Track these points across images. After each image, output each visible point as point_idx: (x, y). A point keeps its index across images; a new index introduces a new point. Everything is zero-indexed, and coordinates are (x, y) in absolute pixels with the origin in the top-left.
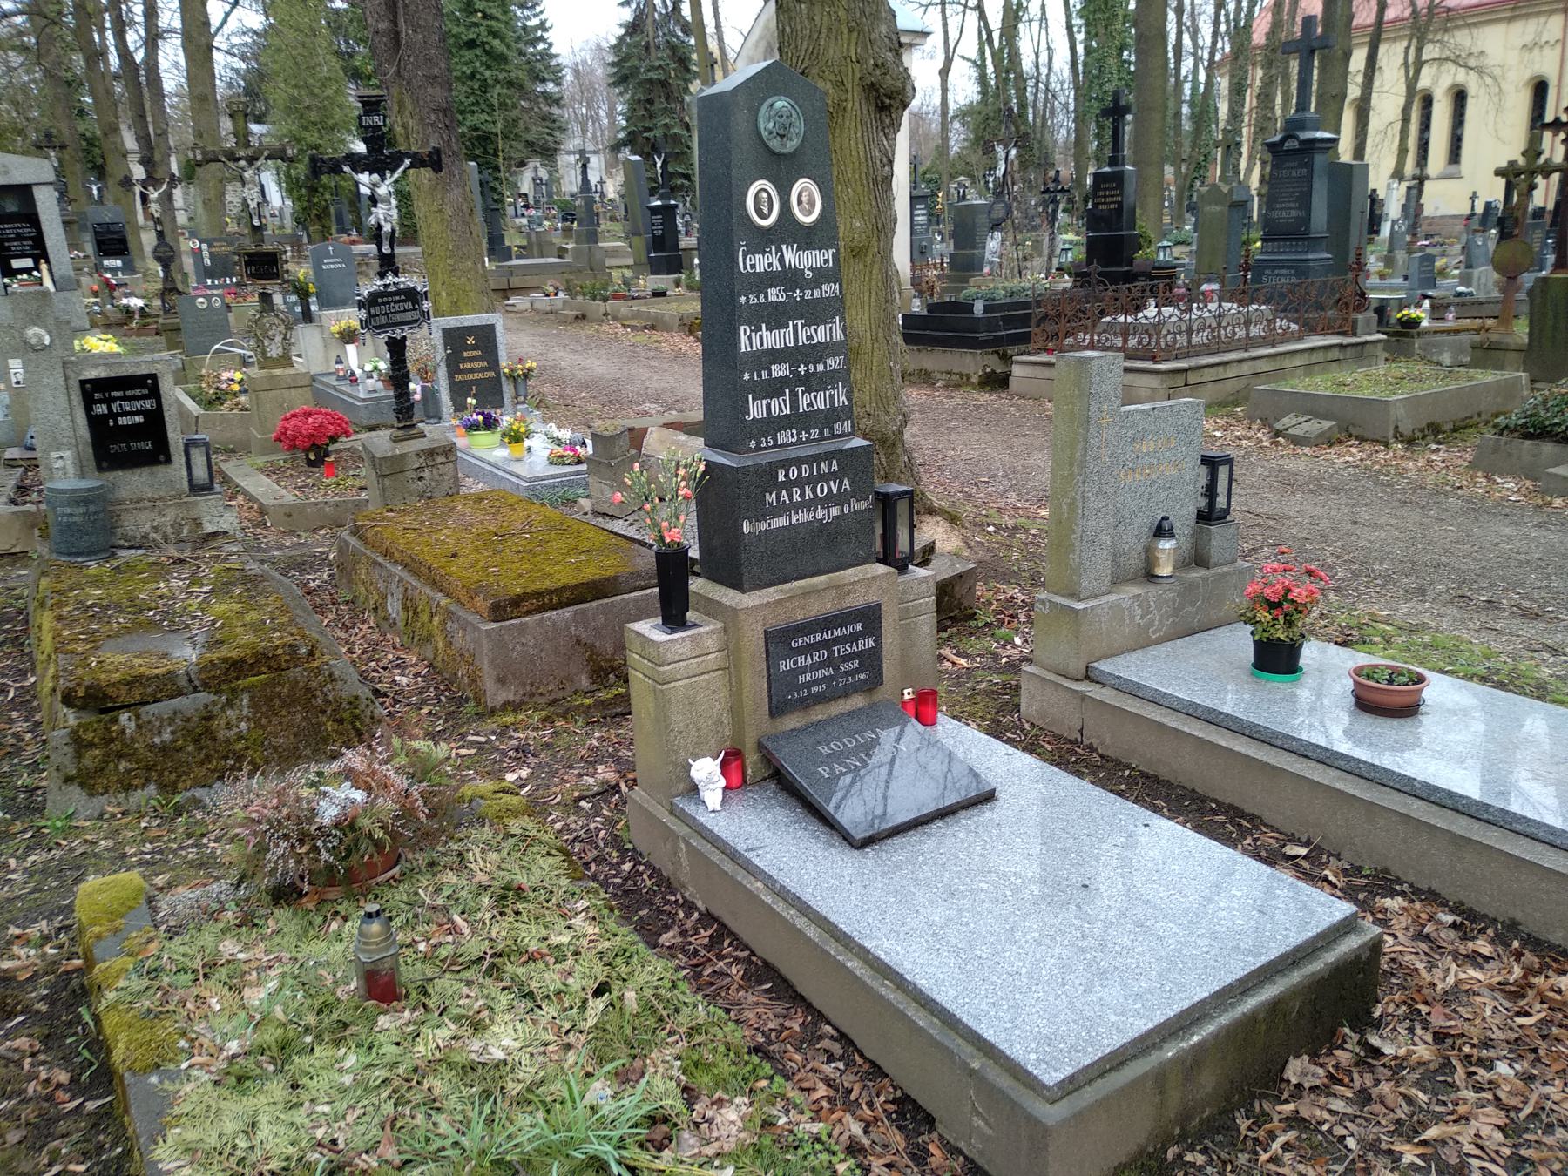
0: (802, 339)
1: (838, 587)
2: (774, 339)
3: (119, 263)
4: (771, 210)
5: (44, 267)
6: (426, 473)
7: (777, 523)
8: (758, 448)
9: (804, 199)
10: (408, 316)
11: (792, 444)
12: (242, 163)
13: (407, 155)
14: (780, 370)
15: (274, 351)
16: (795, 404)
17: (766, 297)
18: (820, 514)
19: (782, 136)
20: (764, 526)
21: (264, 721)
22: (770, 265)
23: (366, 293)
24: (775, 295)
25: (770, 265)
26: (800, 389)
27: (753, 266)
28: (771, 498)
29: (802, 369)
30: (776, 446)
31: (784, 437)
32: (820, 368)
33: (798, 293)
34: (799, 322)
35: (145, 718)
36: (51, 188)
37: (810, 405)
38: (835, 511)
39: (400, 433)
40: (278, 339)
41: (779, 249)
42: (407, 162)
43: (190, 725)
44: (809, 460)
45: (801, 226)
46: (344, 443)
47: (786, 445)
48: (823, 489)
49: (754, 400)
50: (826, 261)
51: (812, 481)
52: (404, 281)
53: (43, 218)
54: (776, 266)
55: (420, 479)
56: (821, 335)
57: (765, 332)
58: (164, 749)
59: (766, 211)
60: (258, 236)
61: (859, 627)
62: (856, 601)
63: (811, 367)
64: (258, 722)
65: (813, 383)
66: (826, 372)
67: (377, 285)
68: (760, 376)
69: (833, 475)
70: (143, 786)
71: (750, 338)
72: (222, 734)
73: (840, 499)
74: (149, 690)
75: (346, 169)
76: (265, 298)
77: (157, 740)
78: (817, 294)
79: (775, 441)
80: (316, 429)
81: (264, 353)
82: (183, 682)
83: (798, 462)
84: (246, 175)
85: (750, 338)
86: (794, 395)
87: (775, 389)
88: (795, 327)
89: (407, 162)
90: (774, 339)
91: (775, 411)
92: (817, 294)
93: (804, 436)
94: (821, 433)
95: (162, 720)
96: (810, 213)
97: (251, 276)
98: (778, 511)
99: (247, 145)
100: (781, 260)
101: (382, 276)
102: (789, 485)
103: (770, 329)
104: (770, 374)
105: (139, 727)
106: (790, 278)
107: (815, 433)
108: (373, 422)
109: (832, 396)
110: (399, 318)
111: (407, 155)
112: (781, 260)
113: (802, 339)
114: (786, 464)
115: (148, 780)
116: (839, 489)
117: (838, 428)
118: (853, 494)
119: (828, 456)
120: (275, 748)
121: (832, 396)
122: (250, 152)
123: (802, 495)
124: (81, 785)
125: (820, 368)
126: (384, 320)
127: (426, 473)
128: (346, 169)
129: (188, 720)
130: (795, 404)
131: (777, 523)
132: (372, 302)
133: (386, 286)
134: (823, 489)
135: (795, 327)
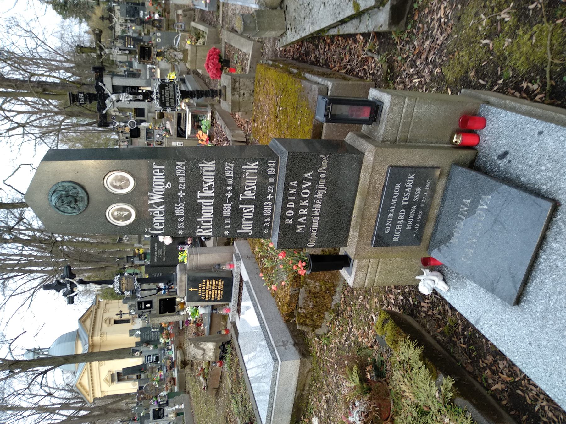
0: (210, 193)
1: (368, 195)
2: (207, 214)
3: (142, 12)
4: (126, 210)
5: (142, 88)
6: (242, 92)
7: (315, 226)
8: (269, 228)
9: (118, 184)
10: (171, 89)
11: (272, 206)
12: (102, 53)
13: (97, 83)
14: (227, 210)
15: (180, 56)
16: (249, 202)
17: (181, 217)
18: (320, 195)
19: (76, 201)
20: (315, 233)
21: (318, 278)
22: (161, 213)
23: (160, 108)
24: (180, 211)
25: (161, 213)
26: (241, 198)
27: (161, 224)
28: (300, 228)
29: (229, 195)
30: (271, 216)
31: (267, 210)
32: (231, 181)
33: (181, 194)
34: (199, 195)
35: (302, 306)
36: (113, 79)
37: (252, 190)
38: (322, 184)
39: (222, 97)
40: (176, 53)
41: (151, 206)
42: (100, 84)
43: (310, 297)
44: (285, 201)
45: (136, 186)
46: (223, 54)
47: (272, 210)
48: (306, 193)
49: (241, 229)
50: (161, 171)
51: (299, 199)
52: (155, 90)
53: (125, 84)
54: (162, 208)
55: (244, 94)
56: (209, 179)
57: (202, 219)
58: (314, 306)
59: (126, 213)
60: (133, 52)
61: (398, 186)
62: (380, 180)
63: (229, 188)
64: (317, 280)
65: (238, 190)
66: (234, 178)
67: (156, 103)
68: (228, 224)
69: (299, 188)
70: (324, 315)
71: (204, 229)
72: (317, 290)
73: (315, 180)
74: (294, 301)
75: (104, 112)
76: (159, 54)
77: (311, 306)
78: (182, 180)
79: (268, 216)
80: (214, 67)
81: (181, 60)
82: (295, 292)
83: (285, 209)
84: (107, 53)
85: (204, 229)
86: (244, 202)
87: (237, 214)
88: (202, 198)
89: (100, 84)
90: (207, 214)
91: (251, 215)
92: (182, 180)
93: (270, 197)
94: (271, 184)
95: (305, 303)
96: (128, 180)
97: (149, 58)
98: (309, 223)
99: (94, 49)
100: (158, 204)
101: (152, 99)
102: (296, 216)
103: (201, 215)
104: (228, 217)
105: (304, 309)
106: (170, 198)
107: (270, 189)
108: (216, 6)
109: (251, 174)
110: (172, 93)
111: (97, 83)
112: (158, 204)
113: (210, 193)
114: (283, 217)
115: (323, 313)
116: (309, 180)
117: (271, 171)
118: (315, 170)
119: (287, 187)
120: (329, 279)
121: (251, 174)
122: (98, 49)
123: (304, 207)
124: (316, 328)
125: (231, 181)
126: (172, 100)
127: (242, 92)
128: (104, 112)
129: (308, 297)
130: (249, 202)
131: (315, 226)
132: (163, 104)
133: (157, 98)
134: (306, 193)
135: (202, 198)
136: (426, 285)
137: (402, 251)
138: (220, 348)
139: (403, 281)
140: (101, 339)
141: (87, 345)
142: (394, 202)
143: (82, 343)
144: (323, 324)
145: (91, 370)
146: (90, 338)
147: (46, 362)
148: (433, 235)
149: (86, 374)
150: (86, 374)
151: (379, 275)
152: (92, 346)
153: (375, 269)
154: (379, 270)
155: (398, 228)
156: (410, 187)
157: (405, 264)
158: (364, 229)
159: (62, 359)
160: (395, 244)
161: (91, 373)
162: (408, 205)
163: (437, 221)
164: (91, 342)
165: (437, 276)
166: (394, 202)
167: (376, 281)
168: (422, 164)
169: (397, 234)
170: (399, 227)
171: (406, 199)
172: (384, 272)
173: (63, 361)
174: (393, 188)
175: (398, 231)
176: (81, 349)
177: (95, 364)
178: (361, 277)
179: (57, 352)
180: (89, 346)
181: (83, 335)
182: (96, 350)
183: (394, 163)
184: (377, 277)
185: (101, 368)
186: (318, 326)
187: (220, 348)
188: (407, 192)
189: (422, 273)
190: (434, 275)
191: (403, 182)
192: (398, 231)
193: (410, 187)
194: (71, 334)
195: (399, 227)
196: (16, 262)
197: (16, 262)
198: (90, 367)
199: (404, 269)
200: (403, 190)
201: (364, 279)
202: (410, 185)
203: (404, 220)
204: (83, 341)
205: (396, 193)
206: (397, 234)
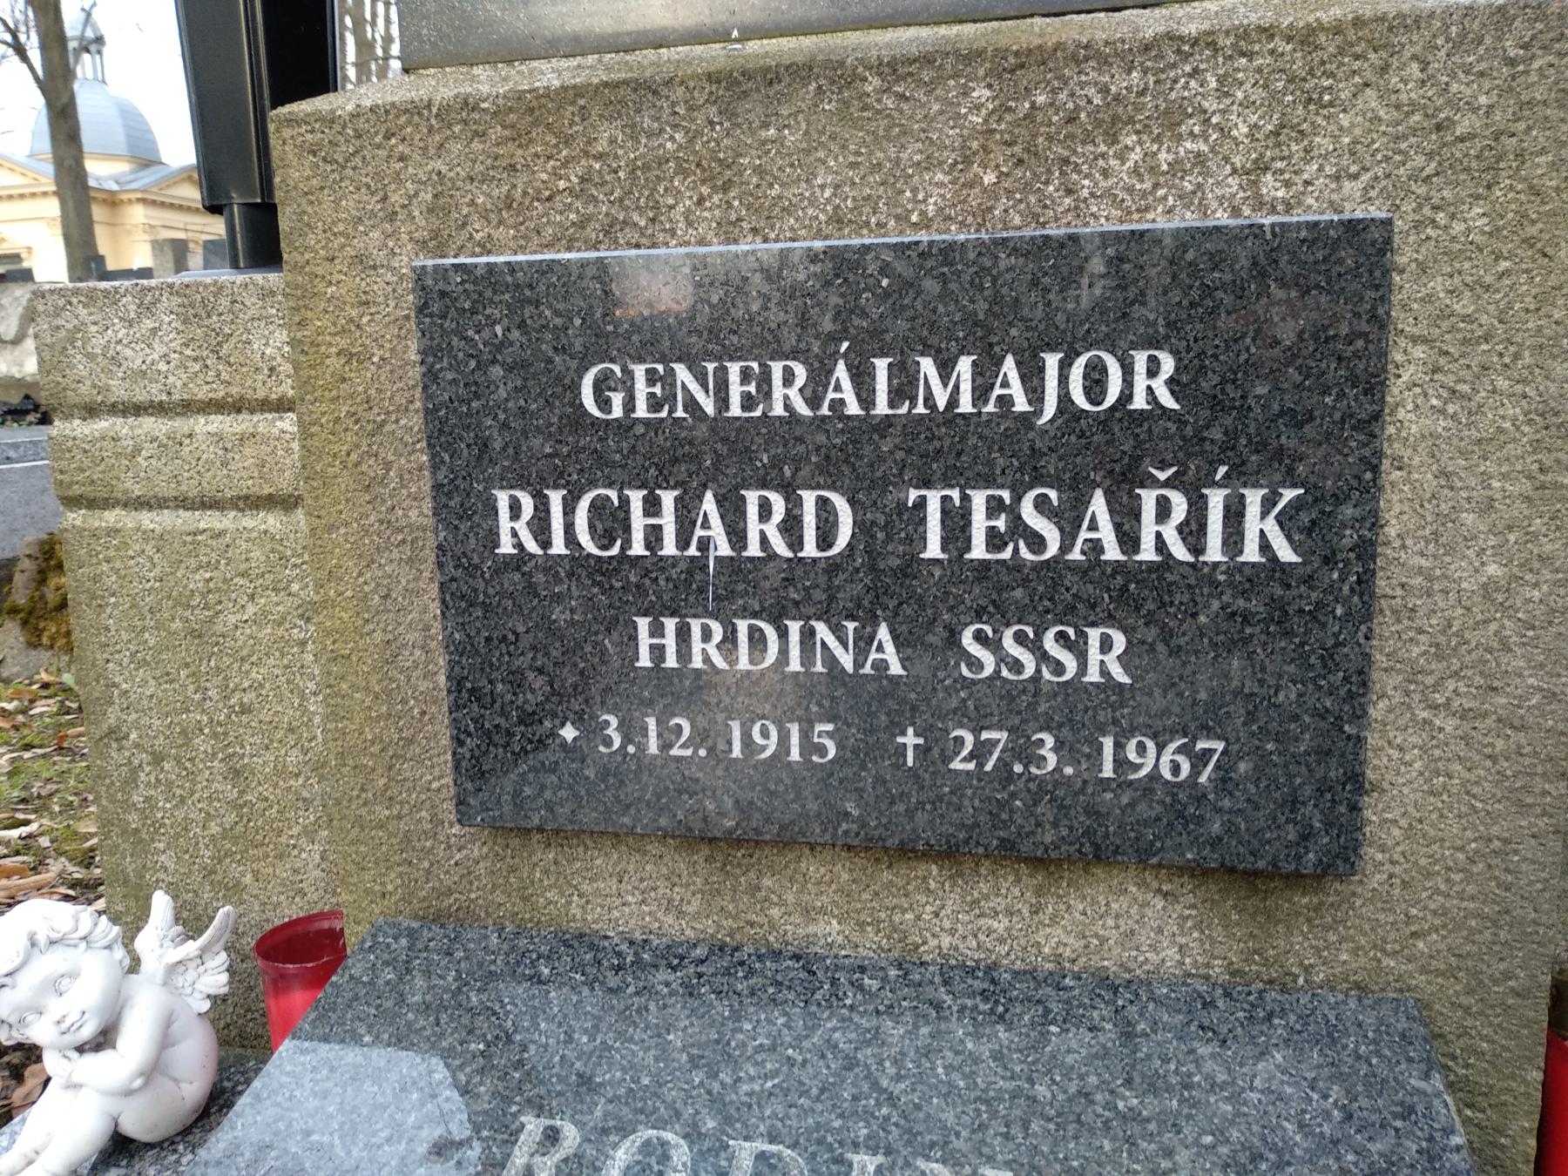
61: (1149, 381)
124: (25, 623)
136: (50, 964)
137: (391, 651)
138: (27, 397)
139: (131, 781)
140: (136, 226)
141: (115, 187)
142: (948, 386)
143: (124, 174)
144: (45, 655)
145: (33, 195)
146: (139, 195)
147: (56, 56)
148: (586, 954)
149: (21, 181)
150: (21, 181)
151: (161, 540)
152: (113, 201)
153: (215, 481)
154: (210, 520)
155: (638, 522)
156: (1129, 540)
157: (281, 771)
158: (606, 134)
159: (64, 99)
160: (462, 509)
161: (22, 196)
162: (912, 564)
163: (728, 970)
164: (125, 197)
165: (154, 1070)
166: (948, 386)
167: (111, 517)
168: (1396, 646)
169: (572, 526)
170: (653, 523)
171: (979, 523)
172: (197, 580)
173: (59, 104)
174: (1116, 327)
175: (611, 523)
176: (99, 171)
177: (52, 207)
178: (134, 358)
179: (89, 102)
180: (112, 193)
181: (148, 177)
182: (98, 212)
183: (1417, 293)
184: (147, 519)
185: (42, 224)
186: (38, 633)
187: (27, 397)
188: (1070, 519)
189: (190, 922)
190: (166, 1040)
191: (1212, 437)
192: (611, 523)
193: (1129, 540)
194: (152, 145)
195: (653, 523)
196: (368, 16)
197: (368, 16)
198: (45, 194)
199: (235, 774)
200: (1108, 453)
201: (119, 390)
202: (1161, 535)
203: (734, 567)
204: (132, 177)
205: (1064, 381)
206: (572, 526)
